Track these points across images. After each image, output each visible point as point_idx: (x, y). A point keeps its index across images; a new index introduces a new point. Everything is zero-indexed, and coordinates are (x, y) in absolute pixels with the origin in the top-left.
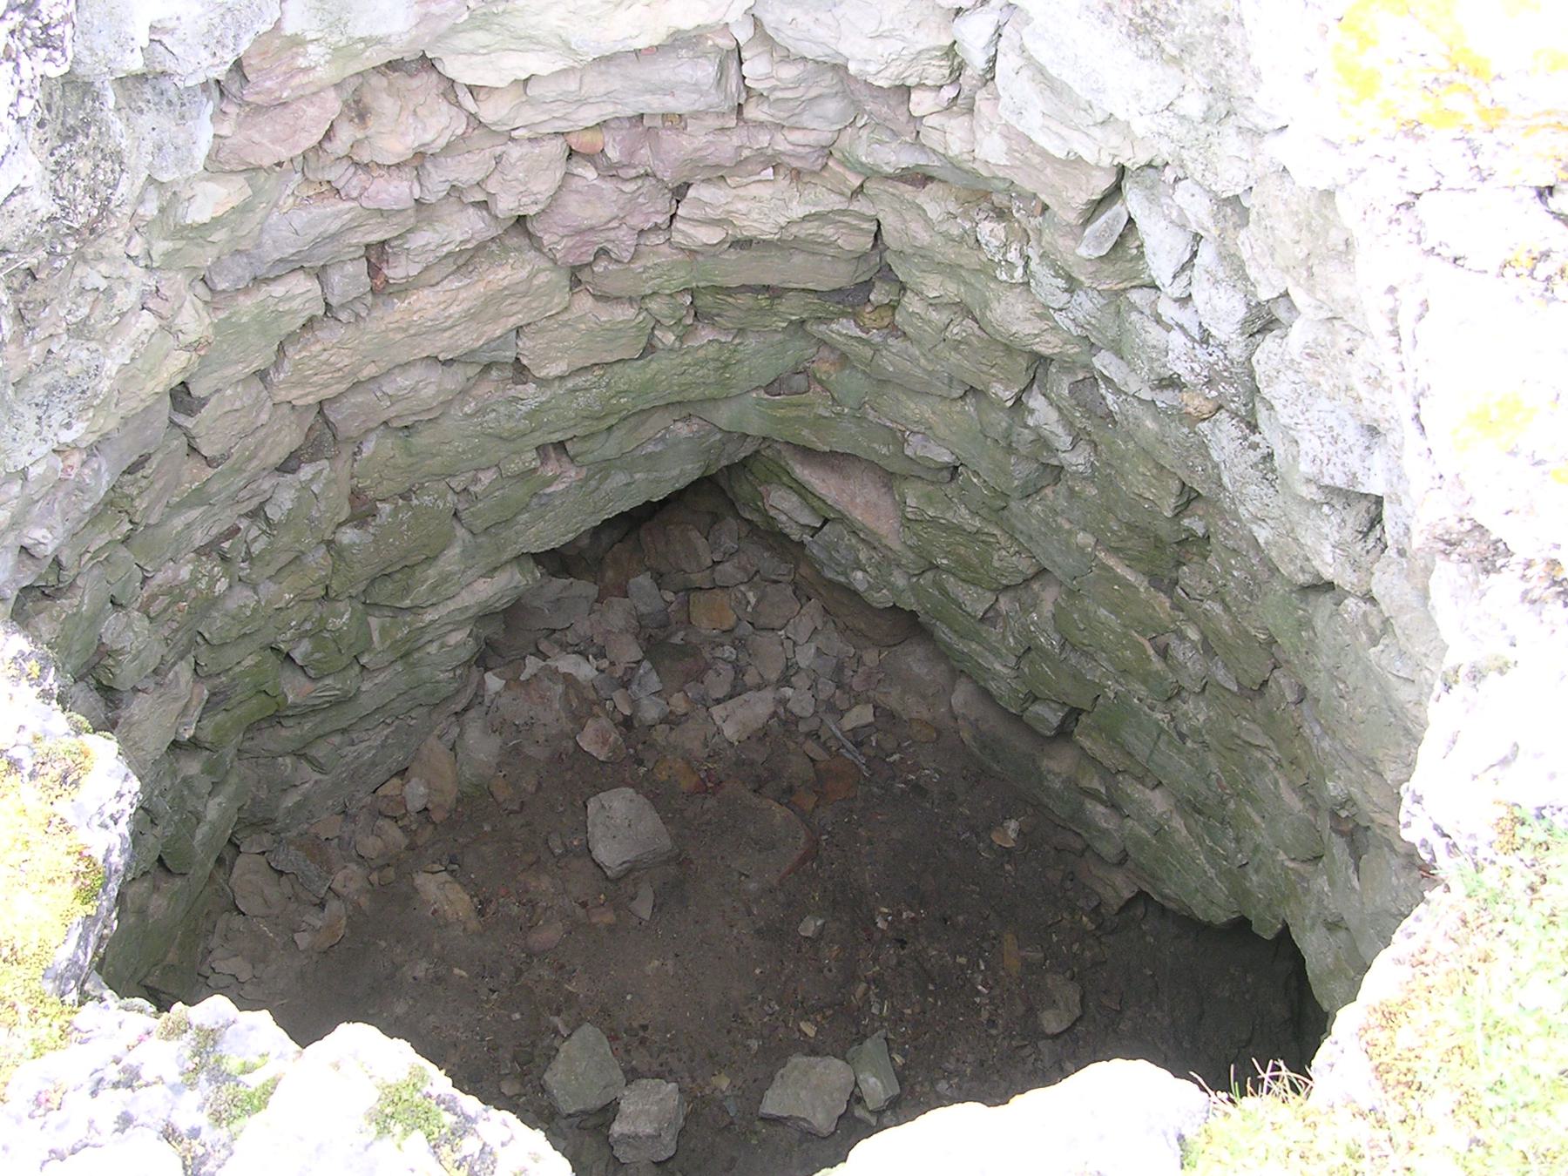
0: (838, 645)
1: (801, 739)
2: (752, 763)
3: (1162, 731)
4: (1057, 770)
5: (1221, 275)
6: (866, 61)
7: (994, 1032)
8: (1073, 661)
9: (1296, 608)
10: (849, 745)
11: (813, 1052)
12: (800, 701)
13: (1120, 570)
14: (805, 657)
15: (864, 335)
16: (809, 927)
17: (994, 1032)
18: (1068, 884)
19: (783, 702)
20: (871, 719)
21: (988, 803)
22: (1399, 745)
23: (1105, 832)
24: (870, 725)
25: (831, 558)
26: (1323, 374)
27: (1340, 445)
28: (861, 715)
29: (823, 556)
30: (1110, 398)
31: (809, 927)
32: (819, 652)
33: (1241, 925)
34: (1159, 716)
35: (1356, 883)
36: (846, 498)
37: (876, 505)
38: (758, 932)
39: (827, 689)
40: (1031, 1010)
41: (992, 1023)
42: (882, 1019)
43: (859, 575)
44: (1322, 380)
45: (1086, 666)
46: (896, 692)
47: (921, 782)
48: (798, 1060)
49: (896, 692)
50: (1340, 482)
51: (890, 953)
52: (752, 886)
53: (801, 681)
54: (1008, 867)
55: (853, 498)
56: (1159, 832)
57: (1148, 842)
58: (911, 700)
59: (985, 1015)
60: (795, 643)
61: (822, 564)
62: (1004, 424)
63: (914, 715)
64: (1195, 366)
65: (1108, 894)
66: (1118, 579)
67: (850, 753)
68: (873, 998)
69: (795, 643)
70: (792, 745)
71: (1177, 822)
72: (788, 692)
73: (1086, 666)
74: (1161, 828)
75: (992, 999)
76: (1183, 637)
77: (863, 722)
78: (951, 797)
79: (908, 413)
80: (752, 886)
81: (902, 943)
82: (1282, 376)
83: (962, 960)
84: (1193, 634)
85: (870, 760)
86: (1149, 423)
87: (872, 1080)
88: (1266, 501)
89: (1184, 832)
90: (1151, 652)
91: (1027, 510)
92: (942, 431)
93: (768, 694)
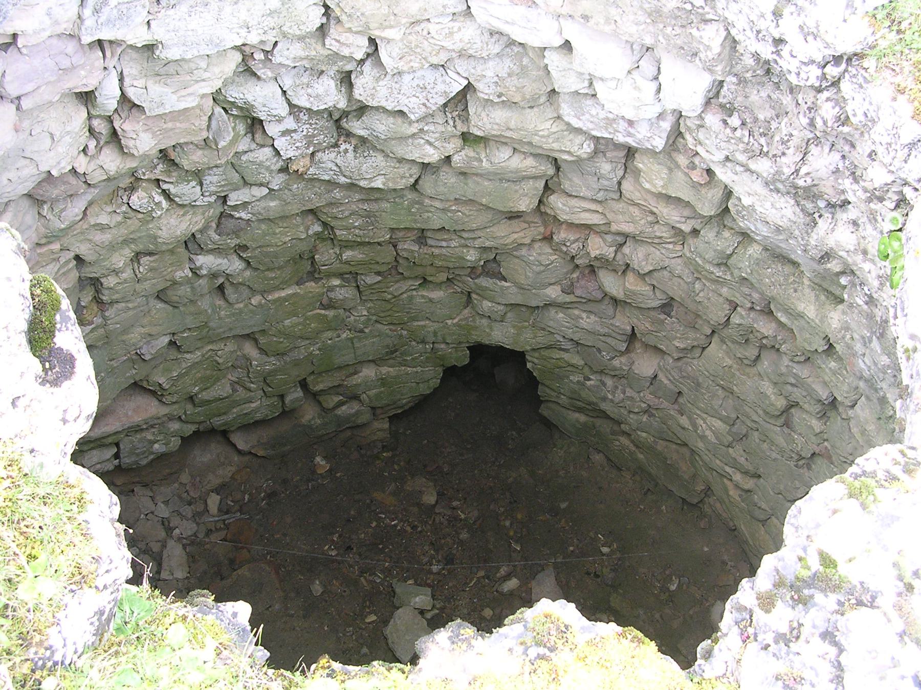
0: (166, 491)
1: (207, 540)
2: (205, 572)
3: (351, 339)
4: (311, 417)
5: (305, 81)
6: (59, 163)
7: (419, 529)
8: (288, 359)
9: (402, 204)
10: (226, 517)
11: (386, 622)
12: (185, 528)
13: (283, 294)
14: (163, 511)
15: (93, 326)
16: (317, 588)
17: (419, 529)
18: (363, 452)
19: (179, 539)
20: (219, 497)
21: (300, 465)
22: (516, 191)
23: (357, 413)
24: (221, 500)
25: (138, 455)
26: (411, 60)
27: (428, 87)
28: (214, 501)
29: (133, 459)
30: (243, 215)
31: (317, 588)
32: (166, 503)
33: (451, 372)
34: (344, 335)
35: (506, 284)
36: (124, 419)
37: (138, 407)
38: (304, 617)
39: (188, 511)
40: (419, 505)
41: (414, 527)
42: (384, 580)
43: (156, 446)
44: (412, 64)
45: (295, 354)
46: (211, 477)
47: (269, 492)
48: (388, 631)
49: (211, 477)
50: (442, 101)
51: (350, 558)
52: (277, 607)
53: (175, 521)
54: (338, 475)
55: (126, 415)
56: (383, 381)
57: (381, 392)
58: (220, 472)
59: (409, 529)
60: (152, 513)
61: (136, 462)
62: (188, 290)
63: (230, 475)
64: (298, 144)
65: (380, 435)
66: (285, 299)
67: (230, 519)
68: (371, 578)
69: (152, 513)
70: (207, 546)
71: (385, 370)
72: (177, 531)
73: (295, 354)
74: (382, 379)
75: (401, 520)
76: (331, 289)
77: (218, 502)
78: (285, 481)
79: (134, 340)
80: (277, 607)
81: (349, 548)
82: (378, 88)
83: (374, 524)
84: (336, 282)
85: (240, 511)
86: (272, 204)
87: (417, 599)
88: (374, 165)
89: (391, 369)
90: (323, 312)
91: (220, 318)
92: (154, 330)
93: (171, 543)
